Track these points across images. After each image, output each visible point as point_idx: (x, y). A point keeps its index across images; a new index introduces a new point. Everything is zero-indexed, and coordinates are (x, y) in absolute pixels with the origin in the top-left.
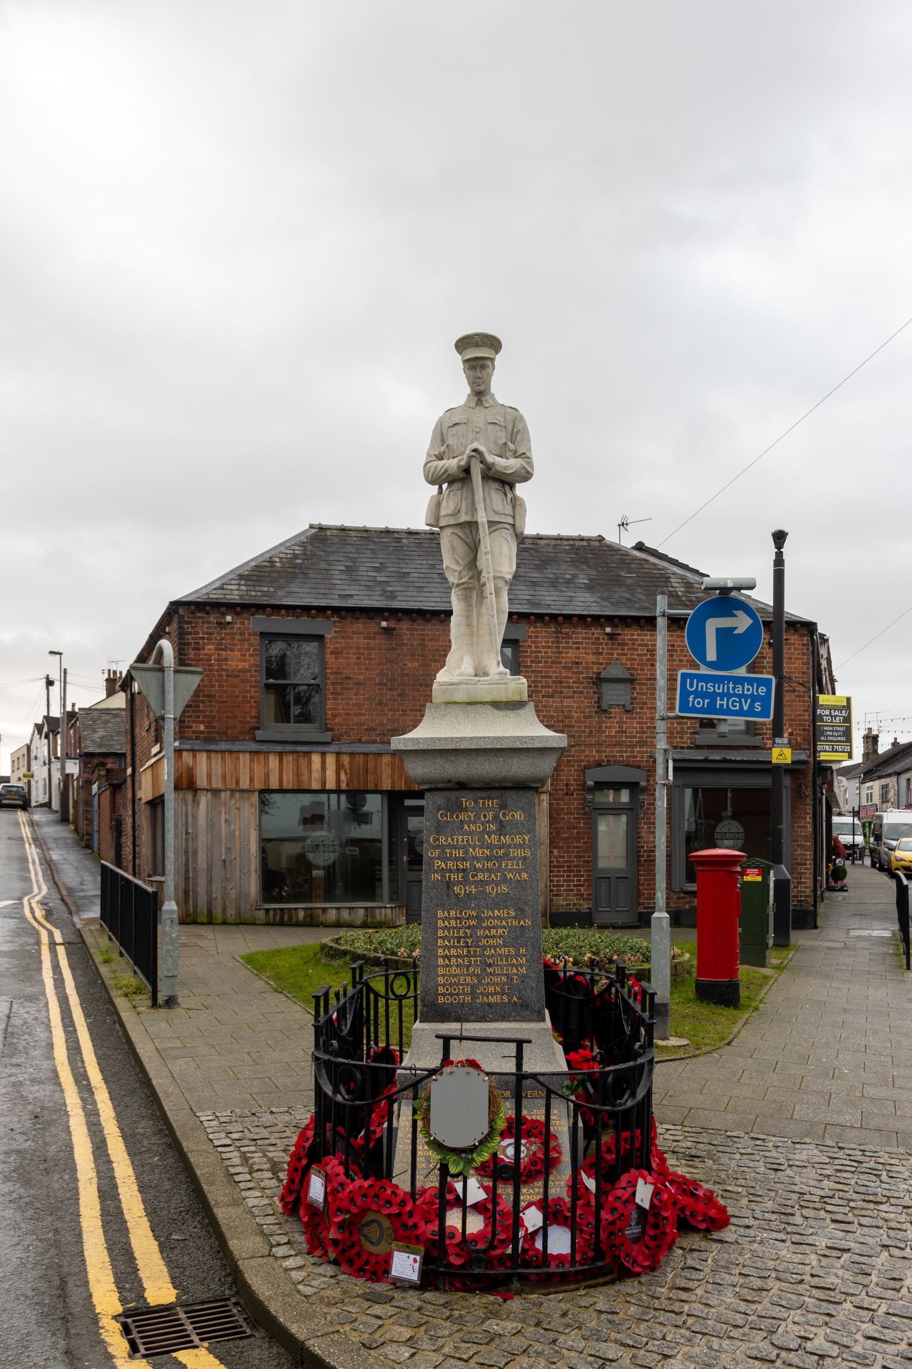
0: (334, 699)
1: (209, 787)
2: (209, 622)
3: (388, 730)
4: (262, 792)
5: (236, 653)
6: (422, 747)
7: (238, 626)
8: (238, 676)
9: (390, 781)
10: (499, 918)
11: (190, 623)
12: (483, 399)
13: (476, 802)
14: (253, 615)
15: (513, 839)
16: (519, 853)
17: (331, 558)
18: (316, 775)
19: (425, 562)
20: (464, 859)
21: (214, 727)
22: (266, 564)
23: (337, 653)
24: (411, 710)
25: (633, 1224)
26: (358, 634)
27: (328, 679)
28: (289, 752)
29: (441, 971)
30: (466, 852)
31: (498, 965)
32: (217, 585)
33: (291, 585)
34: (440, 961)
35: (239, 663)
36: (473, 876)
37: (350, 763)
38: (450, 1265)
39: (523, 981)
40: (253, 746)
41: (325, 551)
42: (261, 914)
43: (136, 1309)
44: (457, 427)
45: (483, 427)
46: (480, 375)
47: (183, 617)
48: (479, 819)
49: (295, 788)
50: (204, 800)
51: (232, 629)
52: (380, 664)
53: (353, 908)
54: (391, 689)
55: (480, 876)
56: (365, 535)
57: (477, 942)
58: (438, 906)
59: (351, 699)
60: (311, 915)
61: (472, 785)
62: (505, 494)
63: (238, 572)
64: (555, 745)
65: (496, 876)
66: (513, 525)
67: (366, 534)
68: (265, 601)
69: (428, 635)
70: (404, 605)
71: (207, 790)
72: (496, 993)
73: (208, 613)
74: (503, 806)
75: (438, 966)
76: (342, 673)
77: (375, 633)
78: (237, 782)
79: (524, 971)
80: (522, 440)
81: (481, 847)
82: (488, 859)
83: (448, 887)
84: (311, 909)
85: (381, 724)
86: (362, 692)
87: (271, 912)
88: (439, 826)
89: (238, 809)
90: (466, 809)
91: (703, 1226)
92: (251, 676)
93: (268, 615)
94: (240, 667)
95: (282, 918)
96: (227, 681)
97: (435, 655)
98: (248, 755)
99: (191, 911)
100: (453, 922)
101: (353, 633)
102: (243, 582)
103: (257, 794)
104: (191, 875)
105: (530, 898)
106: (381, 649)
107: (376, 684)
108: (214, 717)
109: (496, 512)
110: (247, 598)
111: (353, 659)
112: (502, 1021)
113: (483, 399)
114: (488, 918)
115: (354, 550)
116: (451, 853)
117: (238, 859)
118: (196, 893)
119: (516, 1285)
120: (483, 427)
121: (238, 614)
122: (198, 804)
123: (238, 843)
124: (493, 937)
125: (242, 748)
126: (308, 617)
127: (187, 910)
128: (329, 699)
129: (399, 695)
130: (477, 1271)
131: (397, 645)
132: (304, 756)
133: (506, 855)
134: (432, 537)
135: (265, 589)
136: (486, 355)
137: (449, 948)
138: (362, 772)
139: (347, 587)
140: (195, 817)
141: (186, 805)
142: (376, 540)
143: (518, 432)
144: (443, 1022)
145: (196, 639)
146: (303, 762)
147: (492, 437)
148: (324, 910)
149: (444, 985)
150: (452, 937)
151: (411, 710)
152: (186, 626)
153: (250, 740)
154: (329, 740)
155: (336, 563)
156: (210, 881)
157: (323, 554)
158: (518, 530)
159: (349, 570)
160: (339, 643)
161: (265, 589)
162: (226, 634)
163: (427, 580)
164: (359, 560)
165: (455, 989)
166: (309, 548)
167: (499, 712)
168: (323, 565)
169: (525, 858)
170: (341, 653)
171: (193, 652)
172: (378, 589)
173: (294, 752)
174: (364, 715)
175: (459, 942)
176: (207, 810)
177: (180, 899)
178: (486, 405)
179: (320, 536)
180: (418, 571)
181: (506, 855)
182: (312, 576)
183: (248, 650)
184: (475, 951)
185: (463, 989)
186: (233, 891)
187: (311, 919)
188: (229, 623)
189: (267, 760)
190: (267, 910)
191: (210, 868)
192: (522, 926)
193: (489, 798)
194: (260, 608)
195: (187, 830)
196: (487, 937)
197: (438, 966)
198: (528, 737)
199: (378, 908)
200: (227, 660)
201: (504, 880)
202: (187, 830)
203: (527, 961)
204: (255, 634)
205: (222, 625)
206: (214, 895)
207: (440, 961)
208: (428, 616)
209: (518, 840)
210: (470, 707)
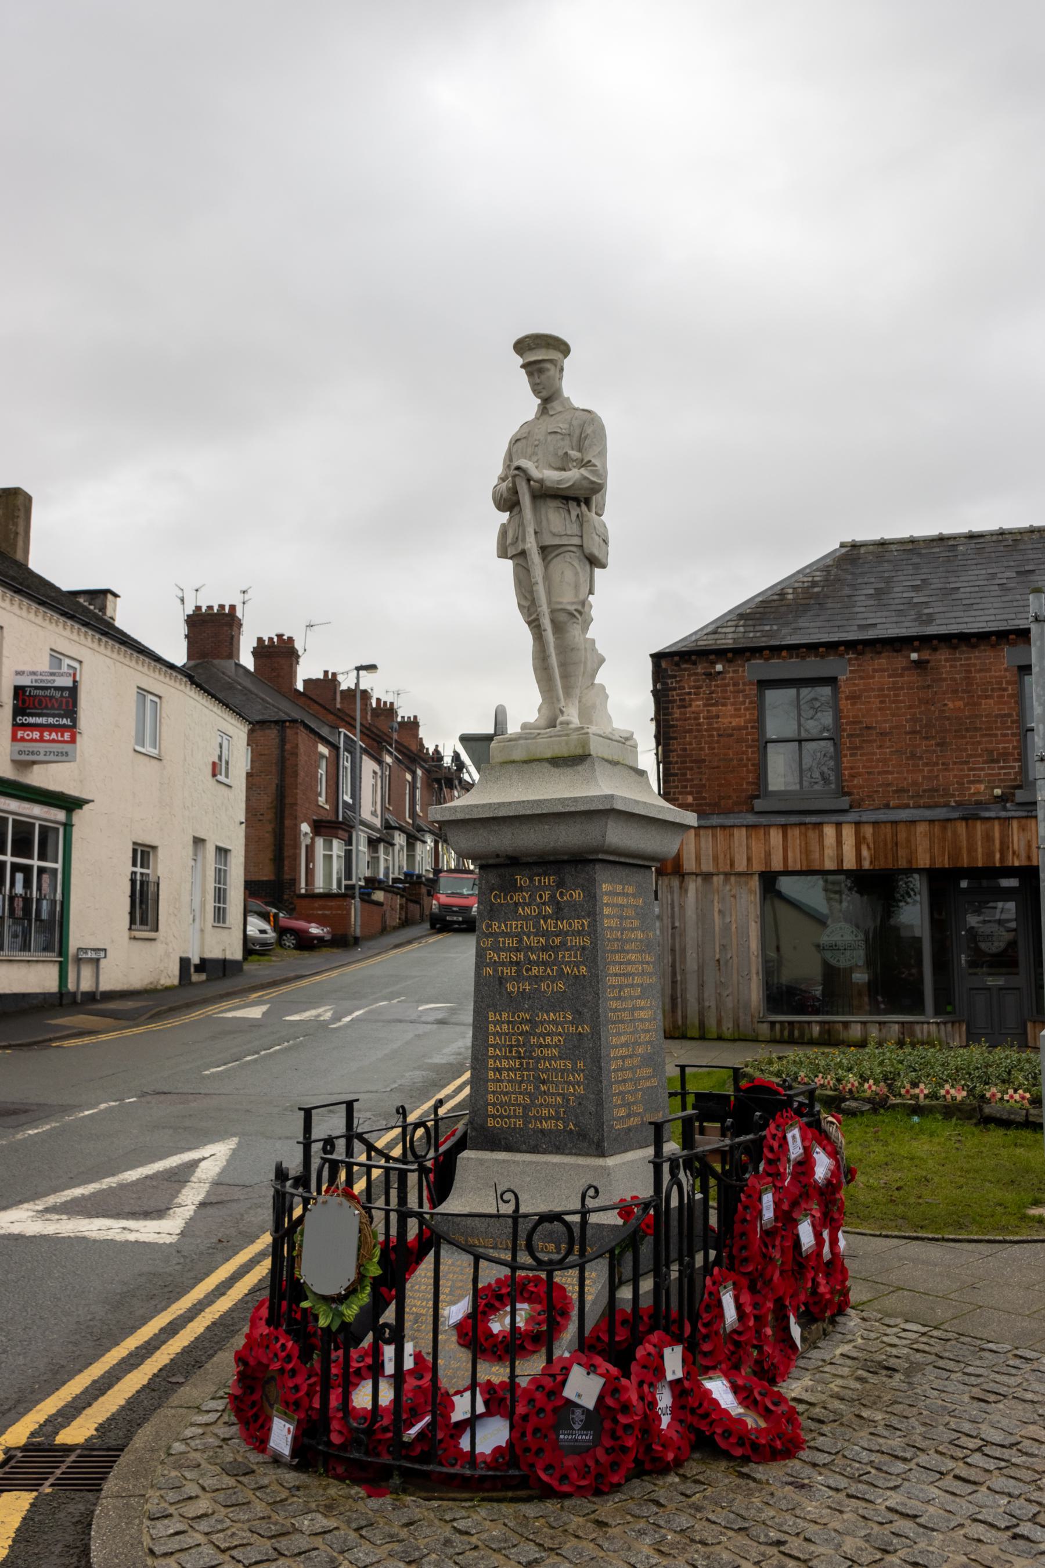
0: (851, 755)
1: (698, 871)
2: (696, 674)
3: (924, 791)
4: (763, 875)
5: (729, 707)
6: (460, 816)
7: (731, 675)
8: (732, 735)
9: (928, 856)
10: (554, 1022)
11: (675, 676)
12: (548, 406)
13: (531, 880)
14: (749, 660)
15: (570, 924)
16: (578, 941)
17: (859, 581)
18: (830, 852)
19: (984, 572)
20: (518, 950)
21: (705, 798)
22: (775, 597)
23: (854, 698)
24: (955, 763)
25: (577, 1427)
26: (881, 672)
27: (844, 730)
28: (795, 825)
29: (491, 1087)
30: (520, 941)
31: (552, 1082)
32: (709, 630)
33: (800, 620)
34: (491, 1074)
35: (732, 720)
36: (527, 970)
37: (874, 835)
38: (329, 1444)
39: (580, 1104)
40: (751, 819)
41: (852, 574)
42: (764, 1029)
43: (39, 1444)
44: (519, 443)
45: (542, 438)
46: (538, 381)
47: (666, 670)
48: (535, 900)
49: (804, 868)
50: (693, 886)
51: (724, 679)
52: (910, 707)
53: (885, 1023)
54: (926, 738)
55: (535, 971)
56: (910, 546)
57: (531, 1052)
58: (489, 1007)
59: (874, 754)
60: (829, 1031)
61: (525, 860)
62: (569, 511)
63: (739, 611)
64: (601, 807)
65: (552, 970)
66: (582, 546)
67: (912, 546)
68: (763, 642)
69: (975, 665)
70: (943, 630)
71: (697, 875)
72: (551, 1118)
73: (694, 663)
74: (560, 884)
75: (488, 1081)
76: (860, 722)
77: (903, 669)
78: (732, 864)
79: (581, 1090)
80: (590, 446)
81: (536, 935)
82: (544, 949)
83: (501, 983)
84: (829, 1023)
85: (915, 783)
86: (888, 744)
87: (778, 1026)
88: (492, 910)
89: (734, 896)
90: (521, 889)
91: (738, 1452)
92: (747, 734)
93: (767, 659)
94: (734, 724)
95: (791, 1033)
96: (718, 742)
97: (986, 690)
98: (744, 831)
99: (680, 1023)
100: (505, 1027)
101: (874, 671)
102: (742, 623)
103: (756, 878)
104: (679, 978)
105: (590, 998)
106: (912, 688)
107: (906, 733)
108: (704, 785)
109: (554, 535)
110: (743, 640)
111: (876, 703)
112: (557, 1153)
113: (548, 406)
114: (542, 1023)
115: (891, 568)
116: (504, 943)
117: (735, 958)
118: (684, 1001)
119: (396, 1481)
120: (542, 438)
121: (730, 661)
122: (686, 891)
123: (734, 941)
124: (548, 1046)
125: (737, 822)
126: (816, 657)
127: (675, 1022)
128: (846, 756)
129: (937, 745)
130: (356, 1455)
131: (933, 680)
132: (814, 829)
133: (563, 944)
134: (1000, 537)
135: (767, 628)
136: (540, 358)
137: (500, 1058)
138: (889, 846)
139: (872, 615)
140: (682, 907)
141: (672, 892)
142: (923, 551)
143: (586, 437)
144: (492, 1150)
145: (681, 694)
146: (813, 835)
147: (551, 449)
148: (846, 1025)
149: (494, 1105)
150: (504, 1046)
151: (955, 763)
152: (669, 681)
153: (747, 811)
154: (847, 807)
155: (864, 586)
156: (701, 986)
157: (849, 577)
158: (587, 551)
159: (879, 593)
160: (855, 685)
161: (767, 628)
162: (716, 686)
163: (982, 595)
164: (895, 579)
165: (505, 1111)
166: (834, 571)
167: (556, 770)
168: (847, 591)
169: (584, 948)
170: (859, 697)
171: (678, 711)
172: (913, 612)
173: (800, 824)
174: (892, 773)
175: (510, 1052)
176: (697, 898)
177: (667, 1008)
178: (551, 413)
179: (853, 556)
180: (971, 584)
181: (563, 944)
182: (829, 605)
183: (744, 703)
184: (528, 1064)
185: (515, 1110)
186: (730, 998)
187: (829, 1035)
188: (719, 673)
189: (767, 834)
190: (773, 1024)
191: (701, 970)
192: (580, 1033)
193: (545, 874)
194: (755, 651)
195: (673, 923)
196: (541, 1046)
197: (488, 1081)
198: (570, 798)
199: (918, 1023)
200: (718, 717)
201: (561, 975)
202: (673, 923)
203: (585, 1078)
204: (751, 683)
205: (711, 676)
206: (707, 1004)
207: (491, 1074)
208: (974, 640)
209: (576, 924)
210: (526, 766)
